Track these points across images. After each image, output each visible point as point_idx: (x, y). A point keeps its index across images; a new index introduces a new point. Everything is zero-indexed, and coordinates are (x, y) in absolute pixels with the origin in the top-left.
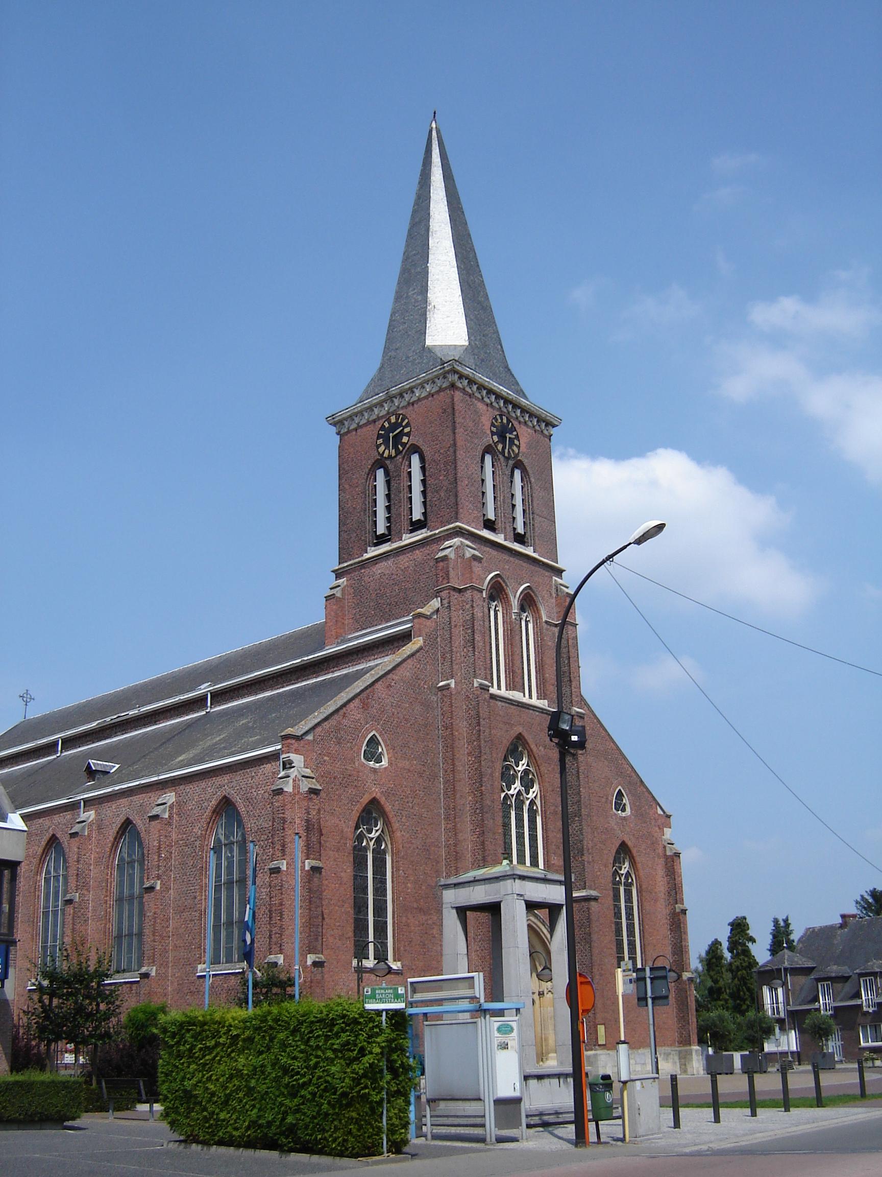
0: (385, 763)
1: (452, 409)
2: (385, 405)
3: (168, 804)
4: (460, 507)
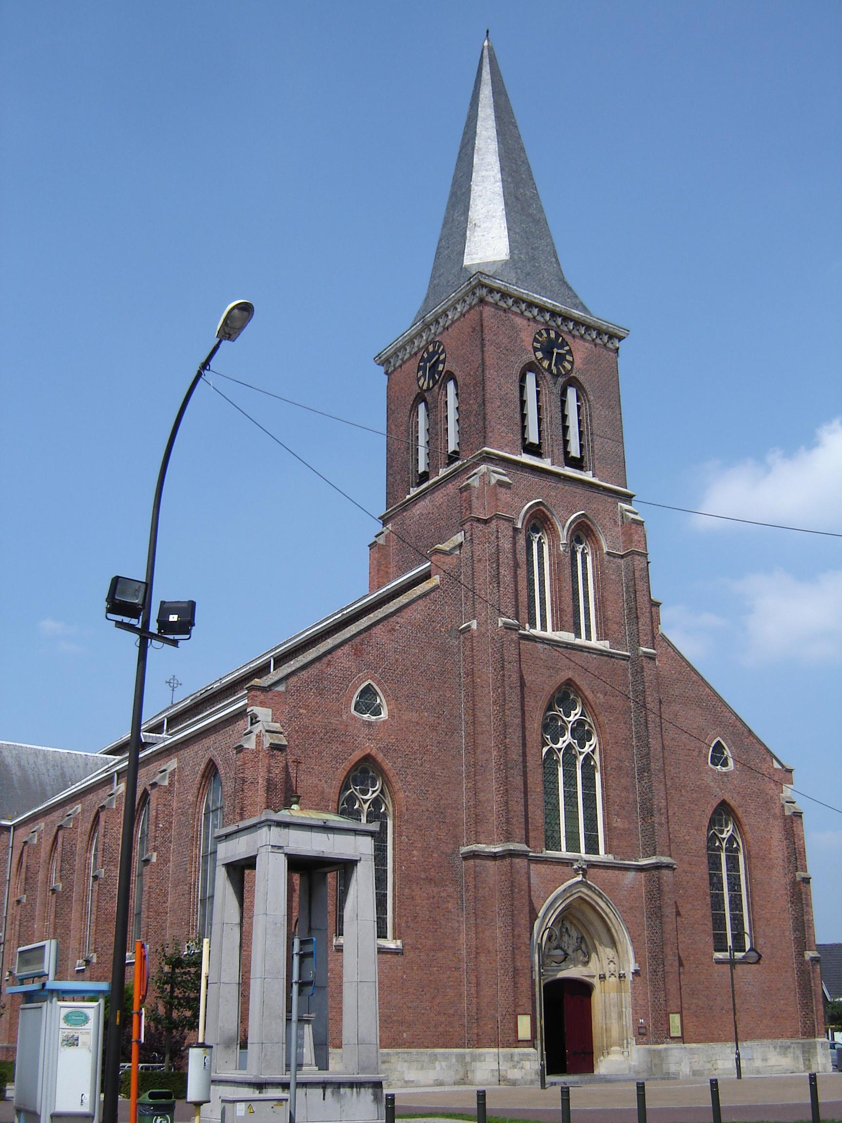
0: (384, 715)
1: (480, 327)
2: (424, 335)
3: (169, 771)
4: (488, 430)
